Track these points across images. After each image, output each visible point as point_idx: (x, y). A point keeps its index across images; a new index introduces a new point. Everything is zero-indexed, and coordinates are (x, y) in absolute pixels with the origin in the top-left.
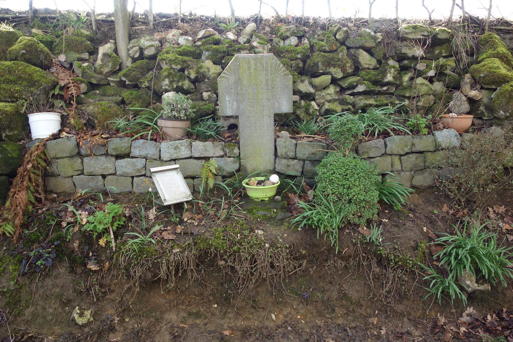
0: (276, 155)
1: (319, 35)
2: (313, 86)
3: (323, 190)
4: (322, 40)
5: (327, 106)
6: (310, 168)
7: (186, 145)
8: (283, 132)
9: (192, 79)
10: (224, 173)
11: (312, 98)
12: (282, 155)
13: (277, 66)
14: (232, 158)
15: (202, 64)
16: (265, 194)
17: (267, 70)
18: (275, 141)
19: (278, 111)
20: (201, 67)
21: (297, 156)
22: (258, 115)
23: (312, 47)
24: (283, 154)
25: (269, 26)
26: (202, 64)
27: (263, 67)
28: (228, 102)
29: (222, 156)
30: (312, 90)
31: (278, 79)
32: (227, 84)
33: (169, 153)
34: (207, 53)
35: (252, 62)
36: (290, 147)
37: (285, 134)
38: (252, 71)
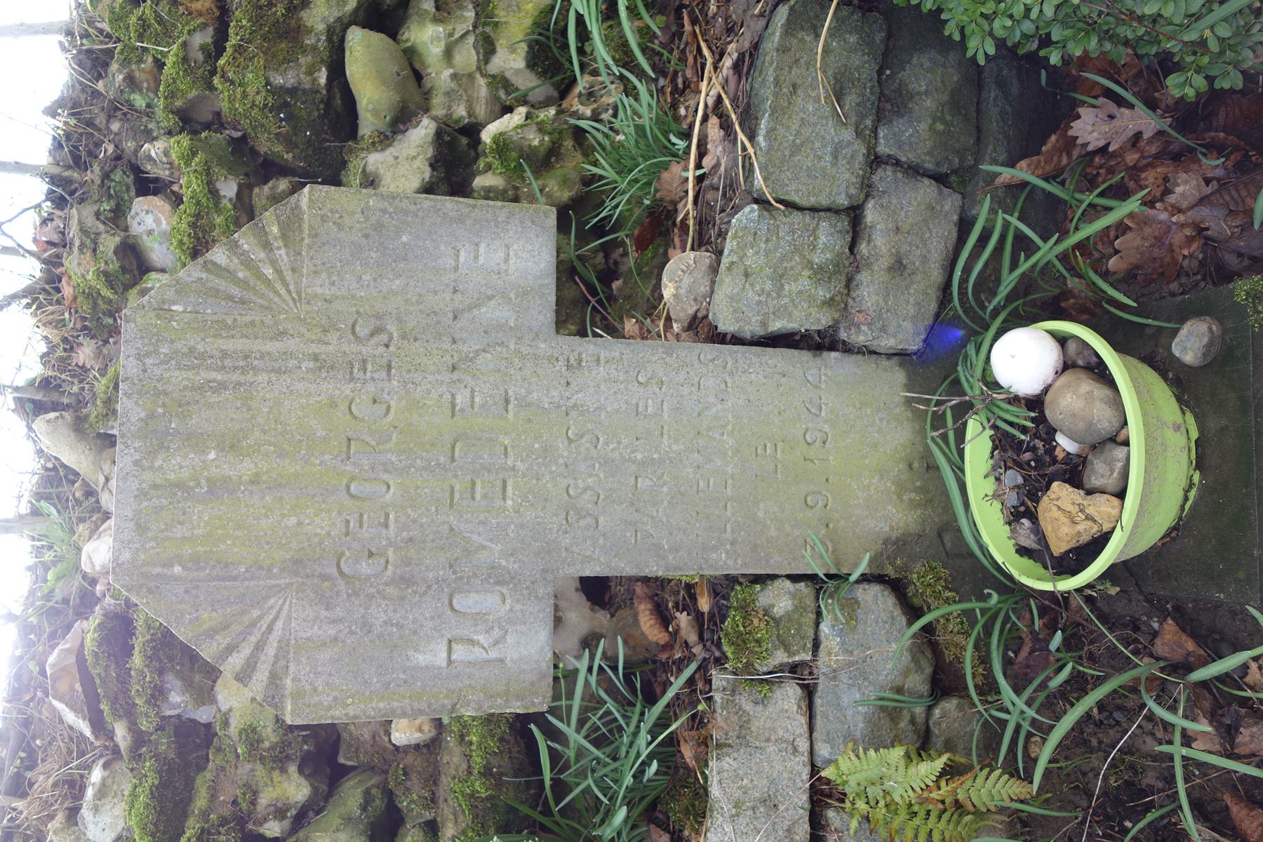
0: (820, 343)
1: (131, 80)
2: (401, 120)
4: (159, 65)
5: (511, 60)
6: (923, 126)
8: (668, 292)
9: (315, 790)
10: (918, 682)
11: (464, 141)
12: (830, 303)
13: (222, 284)
14: (825, 628)
15: (233, 730)
17: (246, 361)
20: (251, 735)
21: (843, 201)
22: (561, 444)
23: (187, 121)
24: (822, 293)
25: (70, 345)
26: (233, 730)
27: (222, 386)
28: (460, 652)
29: (809, 692)
30: (422, 132)
31: (320, 287)
32: (325, 655)
34: (175, 698)
35: (178, 465)
36: (784, 248)
37: (680, 277)
38: (246, 468)
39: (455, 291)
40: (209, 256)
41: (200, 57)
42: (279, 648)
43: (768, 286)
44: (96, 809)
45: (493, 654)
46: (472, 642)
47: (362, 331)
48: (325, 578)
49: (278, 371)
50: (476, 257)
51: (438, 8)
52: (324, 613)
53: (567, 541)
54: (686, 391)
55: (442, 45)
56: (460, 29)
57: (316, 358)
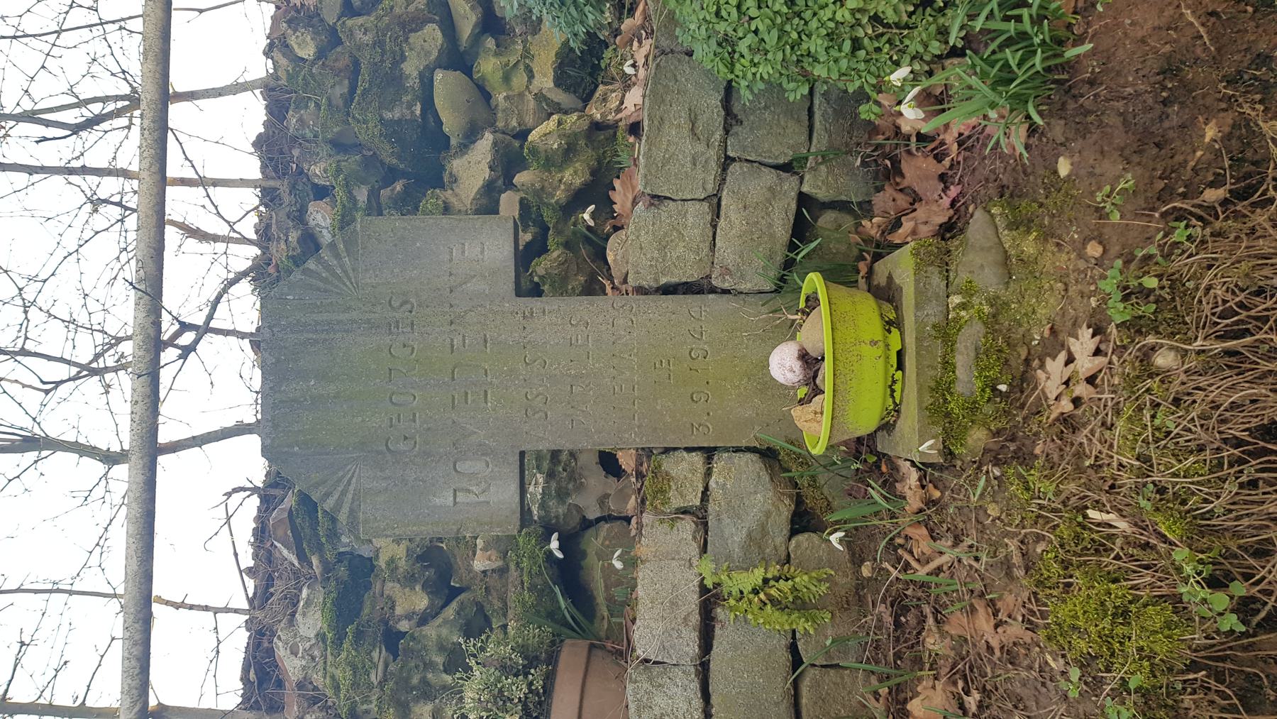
2: (471, 135)
3: (847, 46)
7: (646, 685)
16: (867, 350)
18: (641, 290)
22: (521, 366)
23: (339, 146)
27: (316, 342)
28: (461, 497)
29: (703, 524)
39: (451, 274)
40: (306, 265)
41: (341, 103)
42: (354, 494)
43: (656, 254)
44: (304, 614)
45: (482, 499)
46: (469, 491)
47: (396, 304)
48: (378, 452)
49: (347, 331)
50: (463, 252)
51: (498, 46)
52: (379, 474)
53: (526, 428)
54: (603, 328)
55: (500, 74)
56: (513, 60)
57: (368, 321)
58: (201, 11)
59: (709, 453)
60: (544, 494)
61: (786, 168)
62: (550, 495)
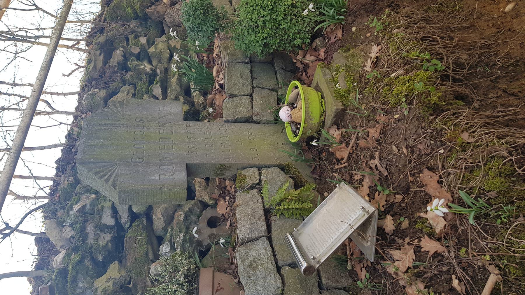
19: (181, 117)
33: (264, 278)
45: (171, 177)
48: (129, 162)
57: (127, 124)
58: (41, 128)
59: (260, 169)
60: (183, 240)
61: (273, 90)
62: (186, 240)
